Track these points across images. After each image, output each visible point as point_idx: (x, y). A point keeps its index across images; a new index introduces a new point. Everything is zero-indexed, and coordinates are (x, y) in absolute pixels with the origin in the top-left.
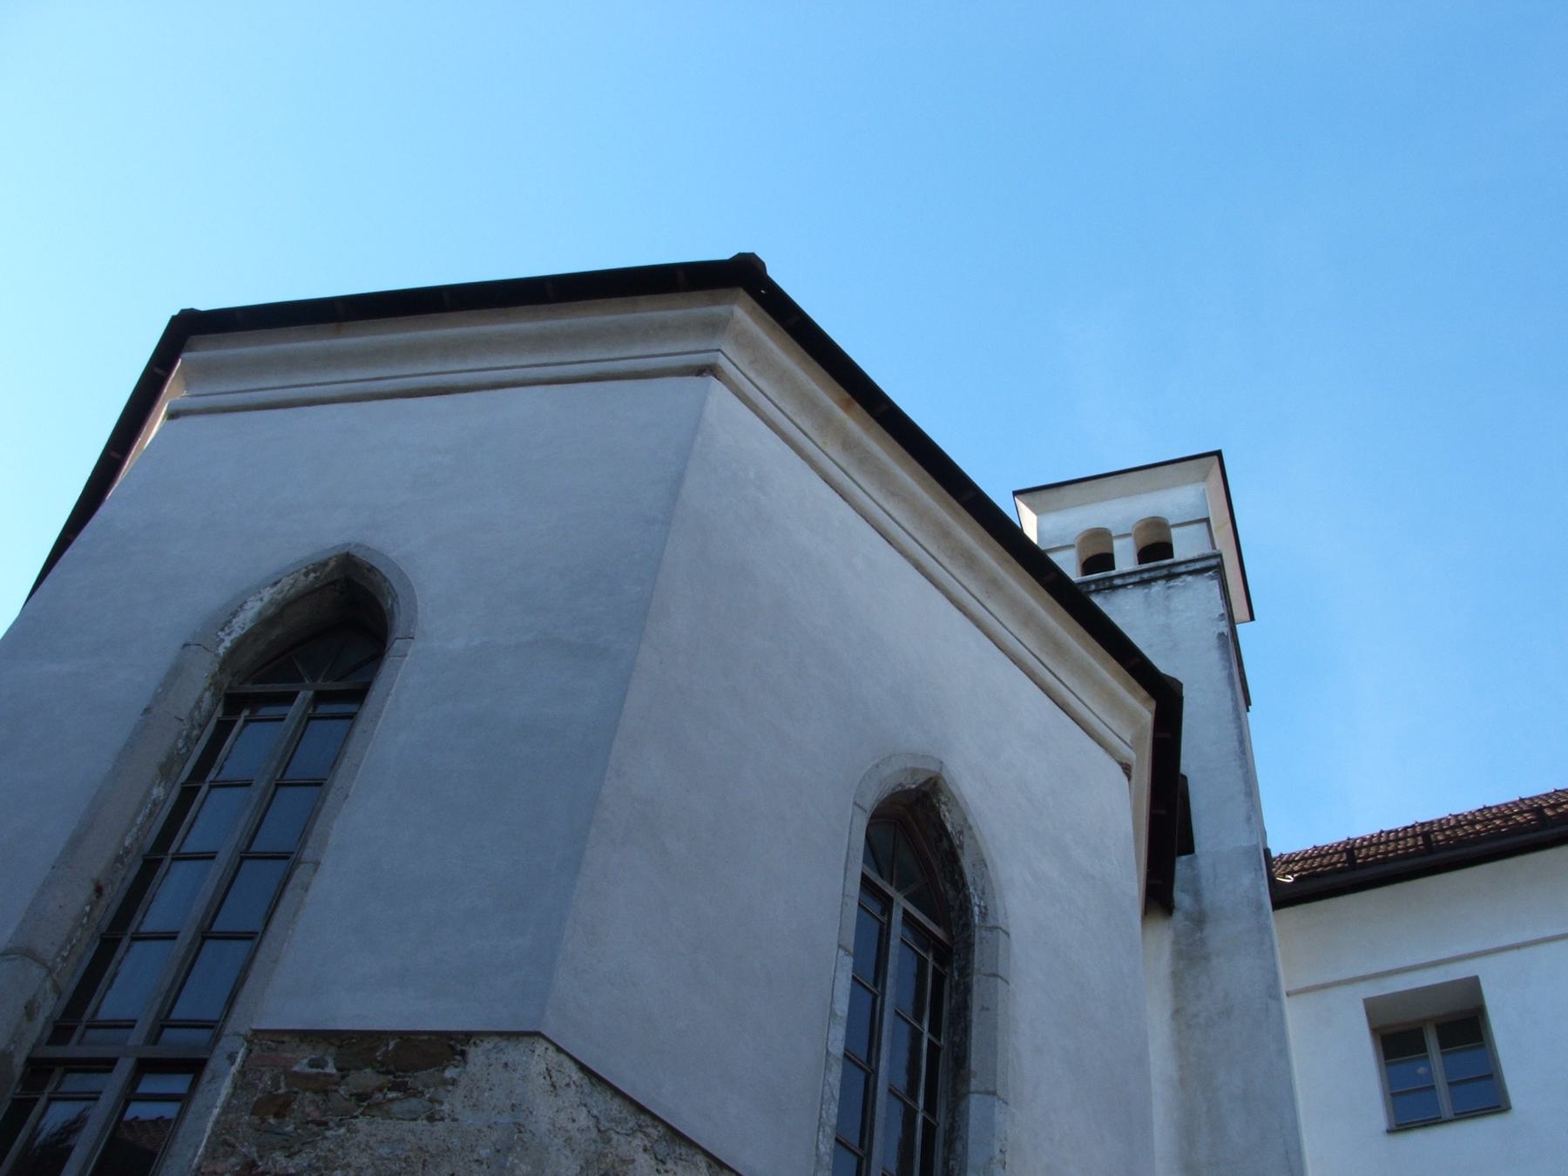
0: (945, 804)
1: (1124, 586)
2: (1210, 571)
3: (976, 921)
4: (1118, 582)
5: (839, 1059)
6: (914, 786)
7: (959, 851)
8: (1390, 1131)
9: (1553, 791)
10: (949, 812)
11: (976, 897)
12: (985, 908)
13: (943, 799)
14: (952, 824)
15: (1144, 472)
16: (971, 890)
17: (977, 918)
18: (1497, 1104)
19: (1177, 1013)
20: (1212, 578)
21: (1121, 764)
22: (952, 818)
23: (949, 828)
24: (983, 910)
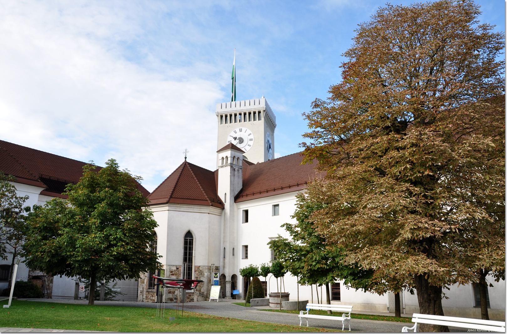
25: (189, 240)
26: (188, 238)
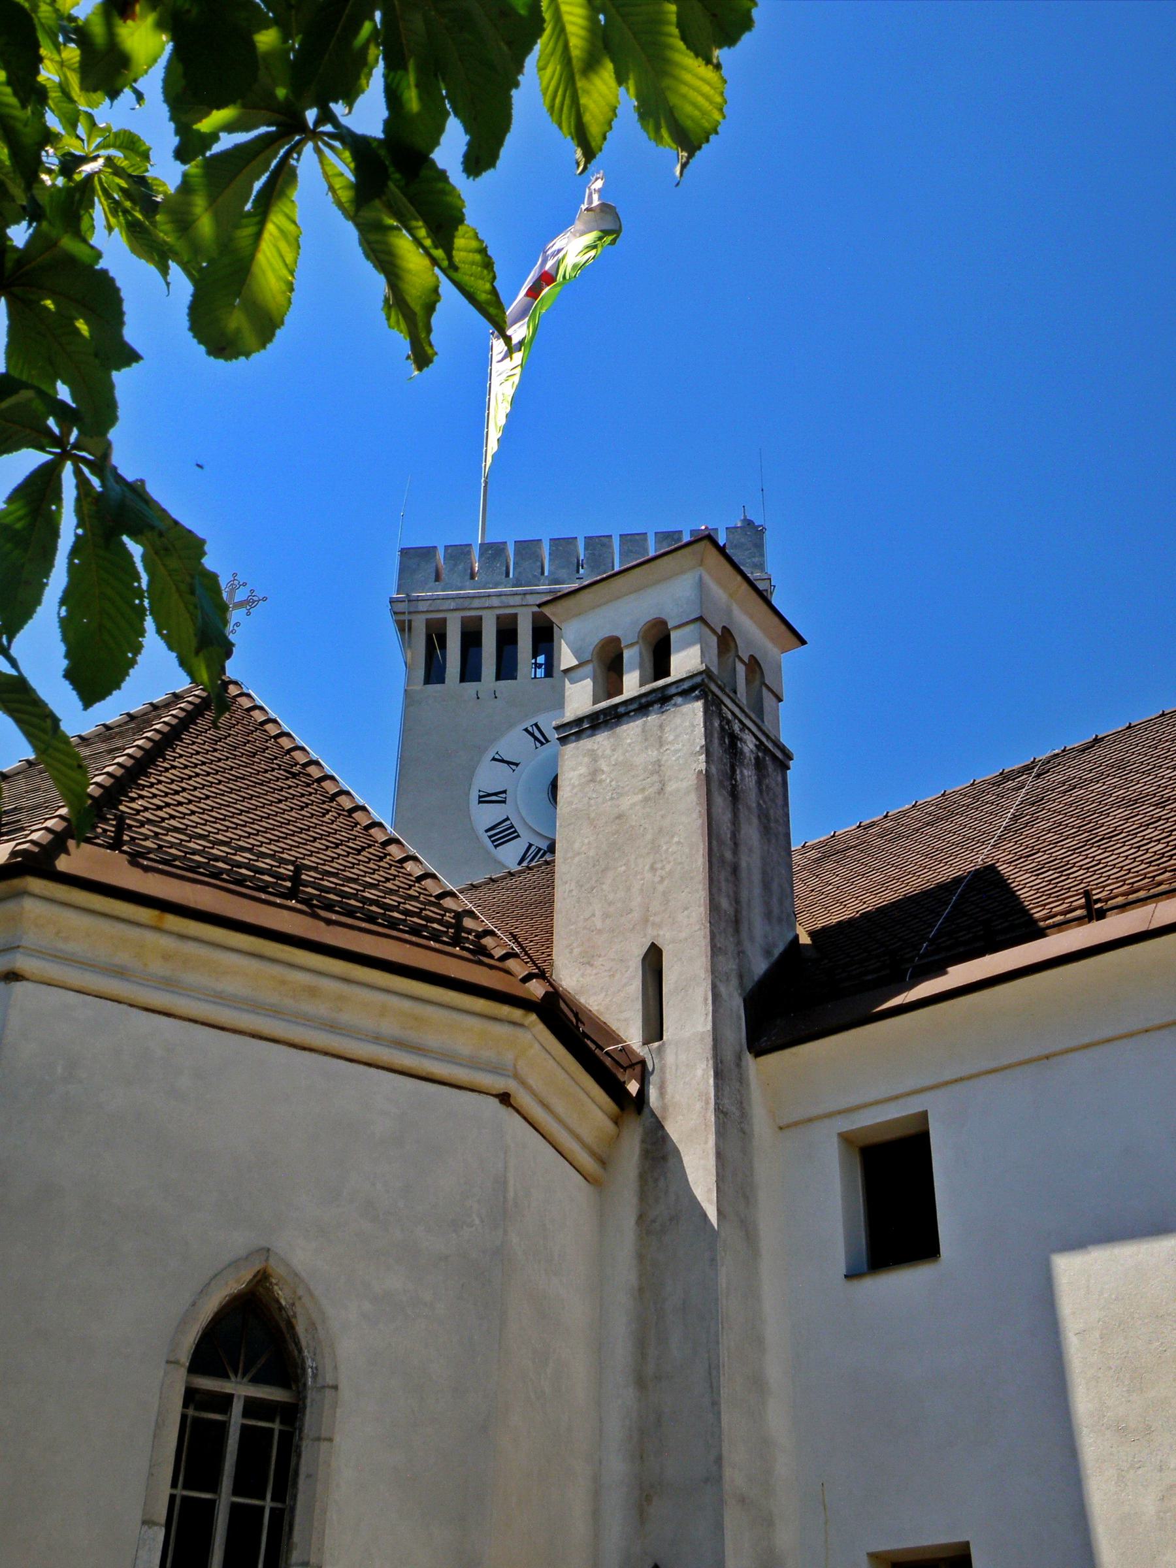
0: (276, 1284)
1: (627, 714)
2: (694, 691)
3: (310, 1383)
4: (622, 710)
5: (577, 994)
7: (293, 1320)
10: (281, 1290)
11: (310, 1360)
12: (316, 1368)
13: (274, 1281)
14: (285, 1299)
15: (644, 567)
16: (306, 1353)
17: (310, 1379)
19: (641, 1218)
20: (697, 698)
21: (496, 1096)
23: (283, 1303)
25: (253, 1408)
26: (240, 1389)
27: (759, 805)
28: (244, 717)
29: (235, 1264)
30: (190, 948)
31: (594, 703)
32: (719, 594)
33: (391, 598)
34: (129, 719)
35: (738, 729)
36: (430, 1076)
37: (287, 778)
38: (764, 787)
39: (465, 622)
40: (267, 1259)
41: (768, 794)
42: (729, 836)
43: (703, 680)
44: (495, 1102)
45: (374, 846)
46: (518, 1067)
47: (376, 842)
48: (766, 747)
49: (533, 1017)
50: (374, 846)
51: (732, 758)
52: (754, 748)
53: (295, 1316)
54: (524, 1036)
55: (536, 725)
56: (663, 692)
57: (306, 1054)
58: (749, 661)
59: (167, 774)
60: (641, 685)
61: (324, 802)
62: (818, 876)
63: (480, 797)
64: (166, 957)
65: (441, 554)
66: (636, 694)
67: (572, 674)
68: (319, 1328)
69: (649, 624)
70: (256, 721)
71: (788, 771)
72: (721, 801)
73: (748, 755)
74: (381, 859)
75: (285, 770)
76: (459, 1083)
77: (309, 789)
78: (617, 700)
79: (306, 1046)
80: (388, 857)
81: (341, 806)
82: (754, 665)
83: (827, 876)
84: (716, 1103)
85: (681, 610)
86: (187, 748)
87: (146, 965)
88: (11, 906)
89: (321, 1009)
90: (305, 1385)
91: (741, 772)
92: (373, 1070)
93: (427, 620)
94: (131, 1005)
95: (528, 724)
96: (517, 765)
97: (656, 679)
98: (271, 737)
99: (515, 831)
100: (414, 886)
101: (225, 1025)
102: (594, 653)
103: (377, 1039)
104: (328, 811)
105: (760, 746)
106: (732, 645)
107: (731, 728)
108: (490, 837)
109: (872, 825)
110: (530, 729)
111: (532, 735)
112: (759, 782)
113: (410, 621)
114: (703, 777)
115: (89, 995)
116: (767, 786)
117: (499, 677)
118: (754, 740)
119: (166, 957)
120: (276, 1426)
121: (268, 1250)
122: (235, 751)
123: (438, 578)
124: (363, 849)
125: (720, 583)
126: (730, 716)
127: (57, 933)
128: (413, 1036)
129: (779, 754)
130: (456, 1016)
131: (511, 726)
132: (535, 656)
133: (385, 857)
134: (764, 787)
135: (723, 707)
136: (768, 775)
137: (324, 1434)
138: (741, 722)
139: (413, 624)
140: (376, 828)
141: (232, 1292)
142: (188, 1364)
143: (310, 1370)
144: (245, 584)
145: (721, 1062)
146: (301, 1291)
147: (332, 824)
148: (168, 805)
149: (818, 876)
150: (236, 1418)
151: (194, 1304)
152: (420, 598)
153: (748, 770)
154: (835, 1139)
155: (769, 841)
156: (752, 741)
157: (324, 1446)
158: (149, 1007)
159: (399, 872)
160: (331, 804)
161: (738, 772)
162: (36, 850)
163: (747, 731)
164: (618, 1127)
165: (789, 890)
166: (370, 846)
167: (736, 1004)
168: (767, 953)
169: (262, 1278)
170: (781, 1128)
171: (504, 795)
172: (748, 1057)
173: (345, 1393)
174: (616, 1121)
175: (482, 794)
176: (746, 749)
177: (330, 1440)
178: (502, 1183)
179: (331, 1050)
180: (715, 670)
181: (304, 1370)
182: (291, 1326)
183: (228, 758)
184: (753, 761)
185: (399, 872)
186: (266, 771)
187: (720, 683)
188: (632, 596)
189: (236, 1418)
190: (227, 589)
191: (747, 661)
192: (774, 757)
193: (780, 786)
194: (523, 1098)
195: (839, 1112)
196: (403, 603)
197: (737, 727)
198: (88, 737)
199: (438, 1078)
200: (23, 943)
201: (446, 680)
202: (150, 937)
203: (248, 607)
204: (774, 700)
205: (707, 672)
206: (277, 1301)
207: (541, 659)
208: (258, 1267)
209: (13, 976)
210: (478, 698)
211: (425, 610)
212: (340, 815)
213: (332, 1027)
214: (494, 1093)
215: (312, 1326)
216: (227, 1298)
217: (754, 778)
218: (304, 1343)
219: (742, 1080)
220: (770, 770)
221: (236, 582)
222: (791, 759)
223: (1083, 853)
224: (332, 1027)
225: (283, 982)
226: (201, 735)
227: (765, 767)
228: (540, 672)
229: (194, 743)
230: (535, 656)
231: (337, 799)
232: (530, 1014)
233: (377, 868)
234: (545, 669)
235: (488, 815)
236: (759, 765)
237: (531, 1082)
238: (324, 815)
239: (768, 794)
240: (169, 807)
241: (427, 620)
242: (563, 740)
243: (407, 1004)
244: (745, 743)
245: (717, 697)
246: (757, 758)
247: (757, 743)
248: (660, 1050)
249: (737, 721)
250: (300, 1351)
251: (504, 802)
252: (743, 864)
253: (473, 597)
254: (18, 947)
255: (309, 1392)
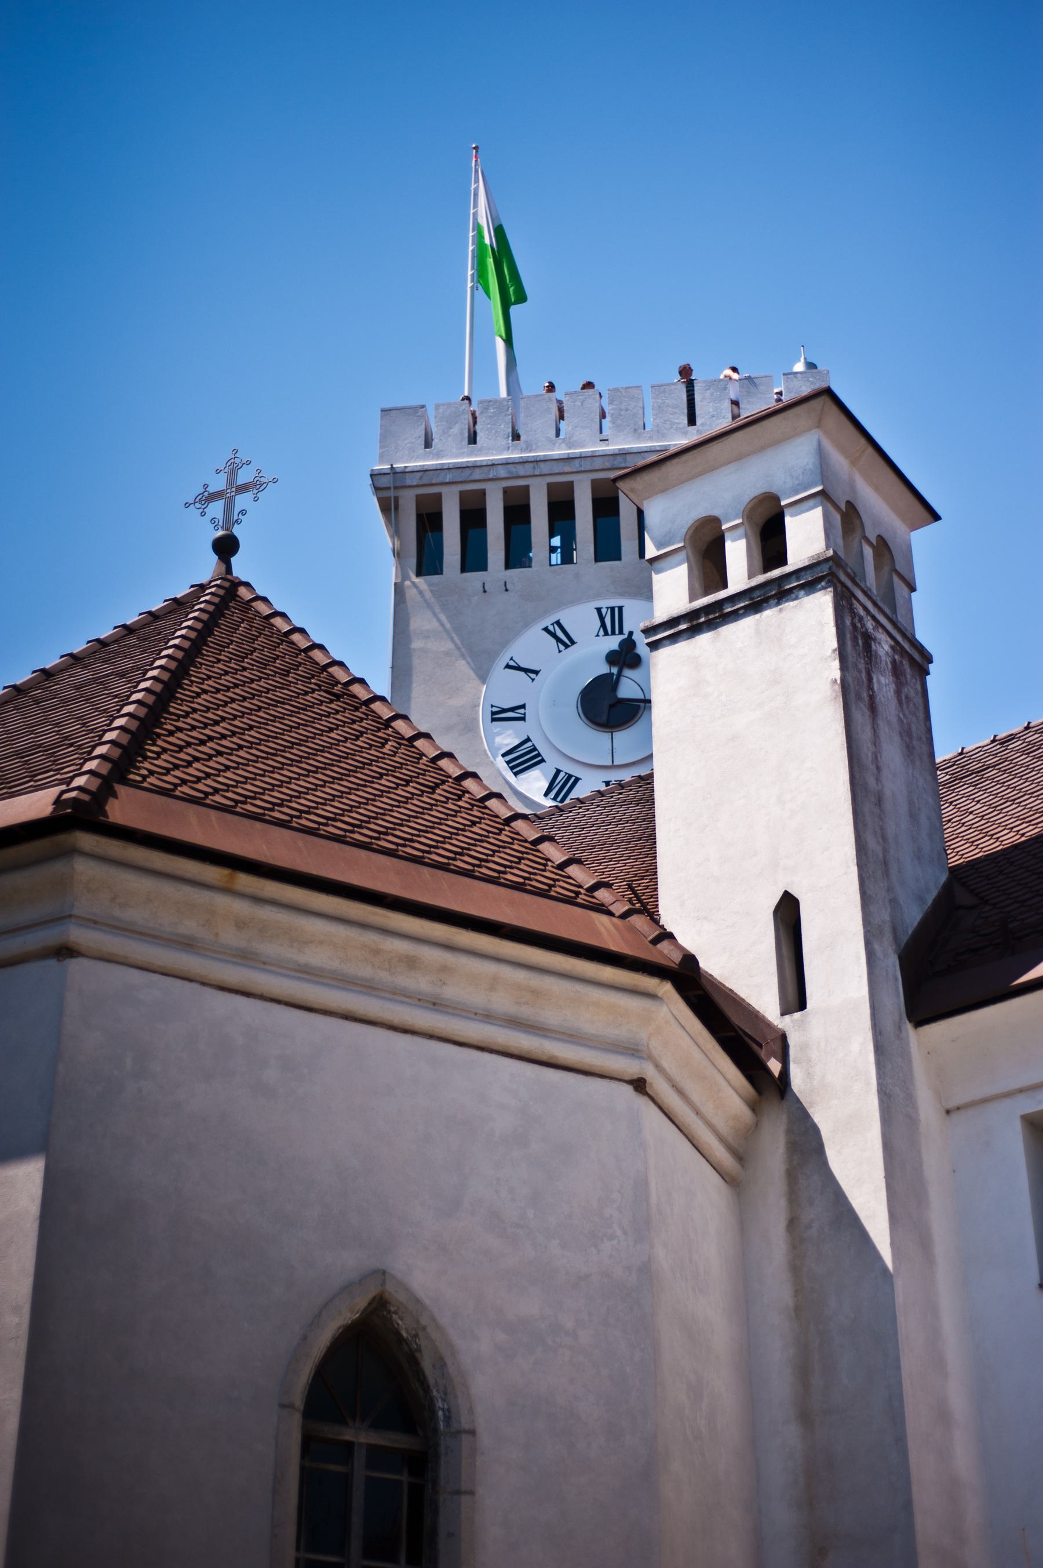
0: (396, 1313)
3: (442, 1428)
6: (358, 1315)
7: (417, 1355)
8: (525, 721)
9: (391, 669)
12: (449, 1410)
13: (392, 1309)
14: (407, 1330)
16: (435, 1393)
17: (441, 1424)
18: (442, 574)
21: (630, 1082)
22: (404, 1324)
23: (405, 1334)
24: (447, 1414)
25: (376, 1455)
27: (900, 720)
28: (265, 627)
29: (348, 1288)
30: (268, 914)
31: (691, 600)
32: (839, 461)
33: (372, 470)
34: (126, 632)
35: (871, 627)
36: (553, 1061)
37: (331, 701)
38: (903, 697)
39: (464, 496)
40: (383, 1284)
41: (908, 707)
42: (870, 759)
43: (830, 568)
44: (629, 1089)
45: (448, 782)
46: (651, 1046)
47: (450, 777)
48: (902, 647)
49: (667, 989)
50: (448, 782)
51: (867, 664)
52: (890, 651)
53: (419, 1350)
54: (662, 1012)
55: (558, 623)
56: (780, 586)
57: (408, 1038)
58: (877, 543)
59: (199, 700)
60: (750, 577)
61: (379, 730)
62: (951, 803)
63: (493, 713)
64: (241, 925)
65: (431, 412)
66: (746, 587)
67: (656, 565)
68: (449, 1363)
69: (755, 501)
70: (280, 631)
71: (928, 677)
72: (861, 716)
73: (883, 658)
74: (460, 798)
75: (325, 691)
76: (587, 1068)
77: (357, 714)
78: (722, 594)
79: (407, 1028)
80: (467, 795)
81: (399, 733)
82: (883, 547)
83: (965, 804)
84: (879, 1084)
85: (797, 482)
86: (213, 667)
87: (217, 935)
88: (58, 867)
89: (421, 983)
90: (436, 1430)
91: (879, 681)
92: (486, 1056)
93: (417, 496)
94: (204, 984)
95: (548, 622)
96: (537, 672)
97: (766, 569)
98: (301, 651)
99: (539, 755)
100: (504, 830)
101: (315, 1006)
102: (688, 537)
103: (488, 1017)
104: (387, 740)
105: (897, 647)
106: (857, 522)
107: (863, 625)
108: (508, 763)
109: (1012, 737)
110: (551, 628)
111: (553, 635)
112: (898, 692)
113: (396, 499)
114: (838, 688)
115: (154, 972)
116: (907, 697)
117: (508, 566)
118: (889, 639)
119: (241, 925)
120: (404, 1478)
121: (384, 1273)
122: (266, 669)
123: (428, 444)
124: (437, 785)
125: (843, 451)
126: (862, 612)
127: (113, 900)
128: (526, 1012)
129: (917, 656)
130: (579, 987)
131: (527, 625)
132: (552, 535)
133: (463, 795)
134: (903, 697)
135: (854, 601)
136: (907, 683)
137: (464, 1487)
138: (874, 618)
139: (401, 502)
140: (446, 759)
141: (345, 1322)
142: (302, 1408)
143: (440, 1413)
144: (248, 463)
145: (880, 1033)
146: (424, 1321)
147: (394, 756)
148: (211, 739)
149: (951, 803)
150: (360, 1472)
151: (305, 1338)
152: (407, 470)
153: (885, 676)
154: (1018, 1126)
155: (913, 762)
156: (887, 641)
157: (465, 1499)
158: (225, 985)
159: (483, 813)
160: (387, 732)
161: (875, 680)
162: (86, 797)
163: (880, 630)
164: (756, 1115)
165: (938, 824)
166: (443, 782)
167: (892, 964)
168: (921, 899)
169: (380, 1305)
170: (948, 1112)
171: (522, 711)
172: (909, 1026)
173: (485, 1439)
174: (754, 1107)
175: (495, 709)
176: (881, 652)
177: (472, 1493)
178: (641, 1185)
179: (437, 1032)
180: (841, 554)
181: (433, 1412)
182: (414, 1362)
183: (261, 678)
184: (890, 666)
185: (483, 813)
186: (306, 693)
187: (849, 571)
188: (732, 467)
189: (360, 1472)
190: (226, 470)
191: (875, 543)
192: (911, 659)
193: (920, 695)
194: (659, 1085)
195: (1021, 1091)
196: (388, 476)
197: (870, 624)
198: (81, 656)
199: (561, 1062)
200: (76, 912)
201: (445, 570)
202: (222, 901)
203: (255, 491)
204: (906, 590)
205: (835, 559)
206: (398, 1333)
207: (556, 541)
208: (372, 1292)
209: (66, 952)
210: (485, 591)
211: (415, 484)
212: (400, 744)
213: (436, 1004)
214: (627, 1078)
215: (441, 1363)
216: (341, 1330)
217: (893, 687)
218: (431, 1381)
219: (906, 1055)
220: (908, 676)
221: (237, 461)
222: (931, 662)
223: (1031, 755)
224: (436, 1004)
225: (377, 952)
226: (224, 651)
227: (904, 674)
228: (556, 558)
229: (219, 661)
230: (552, 535)
231: (393, 724)
232: (664, 983)
233: (458, 809)
234: (562, 553)
235: (508, 737)
236: (896, 671)
237: (665, 1064)
238: (383, 745)
239: (908, 707)
240: (212, 741)
241: (417, 496)
242: (654, 646)
243: (521, 976)
244: (880, 643)
245: (847, 588)
246: (894, 662)
247: (892, 643)
248: (802, 1023)
249: (869, 618)
250: (427, 1389)
251: (523, 719)
252: (888, 793)
253: (474, 467)
254: (70, 916)
255: (442, 1438)
